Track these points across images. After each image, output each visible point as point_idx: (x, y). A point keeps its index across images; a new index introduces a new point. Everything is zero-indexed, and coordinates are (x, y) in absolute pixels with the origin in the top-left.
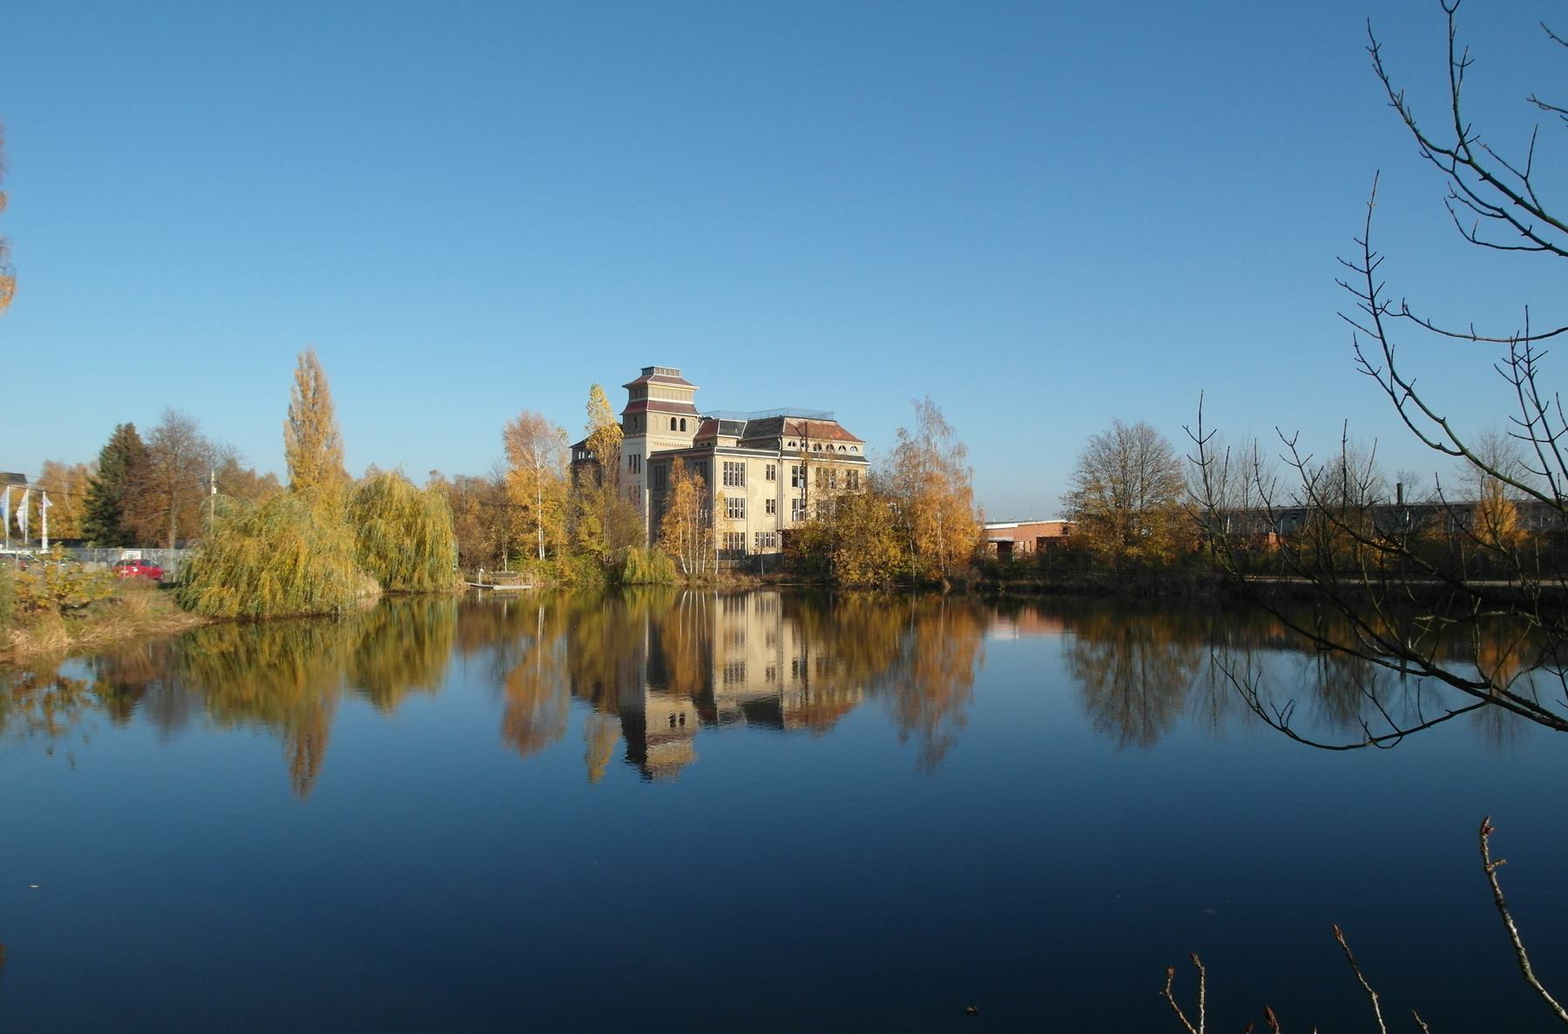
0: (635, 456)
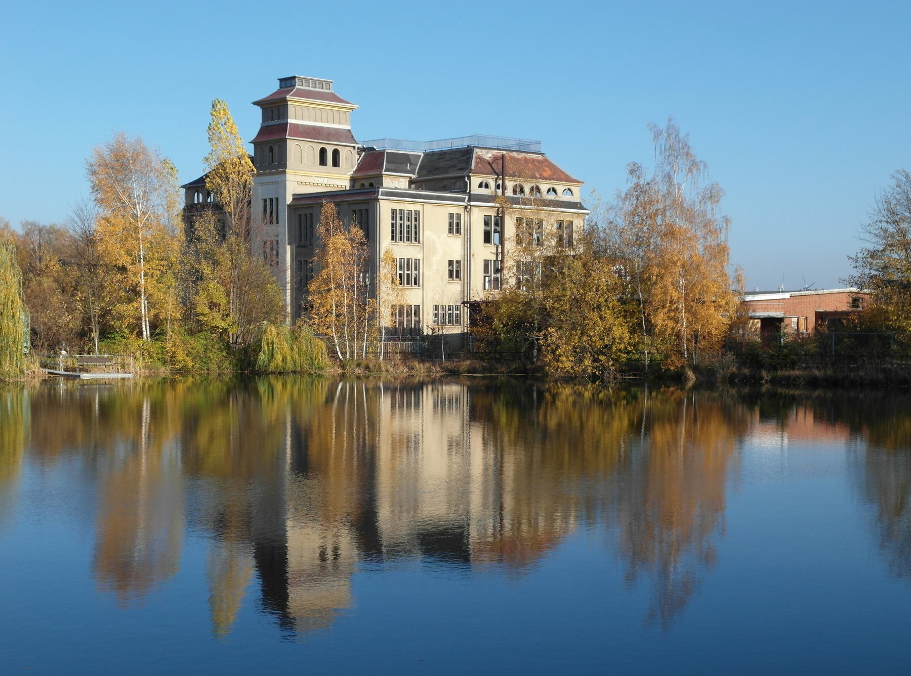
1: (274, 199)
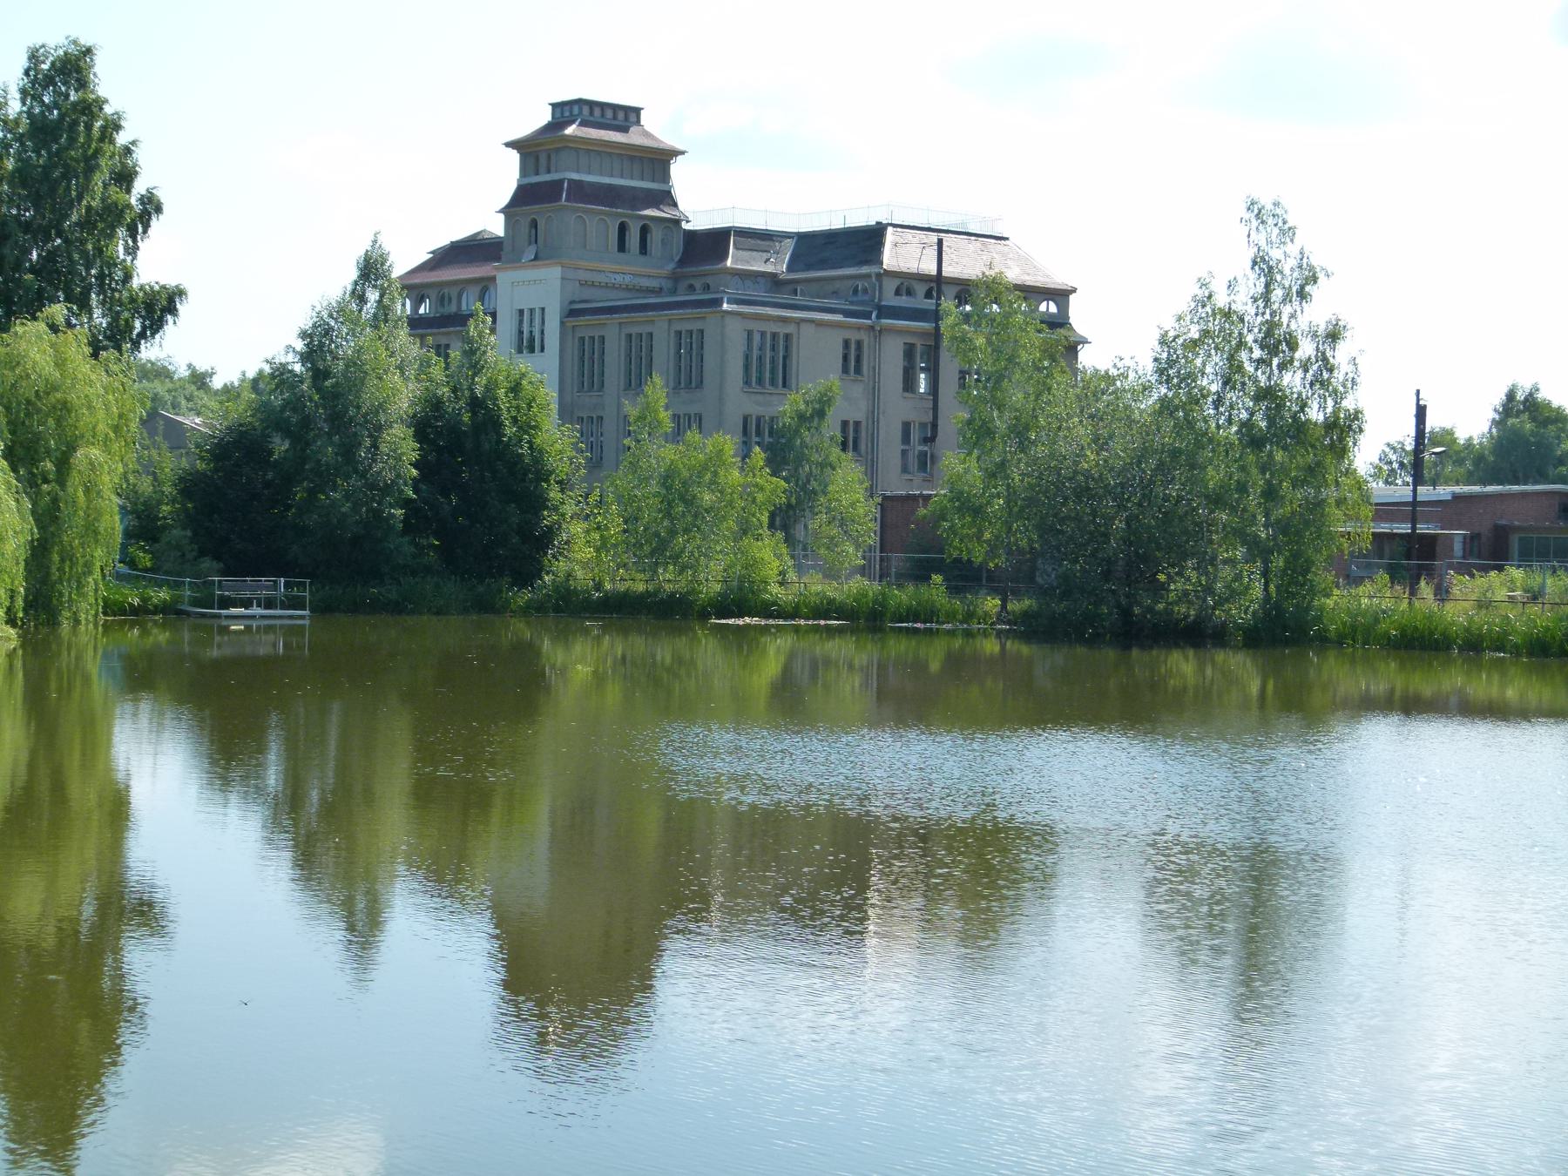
0: (760, 381)
1: (537, 310)
